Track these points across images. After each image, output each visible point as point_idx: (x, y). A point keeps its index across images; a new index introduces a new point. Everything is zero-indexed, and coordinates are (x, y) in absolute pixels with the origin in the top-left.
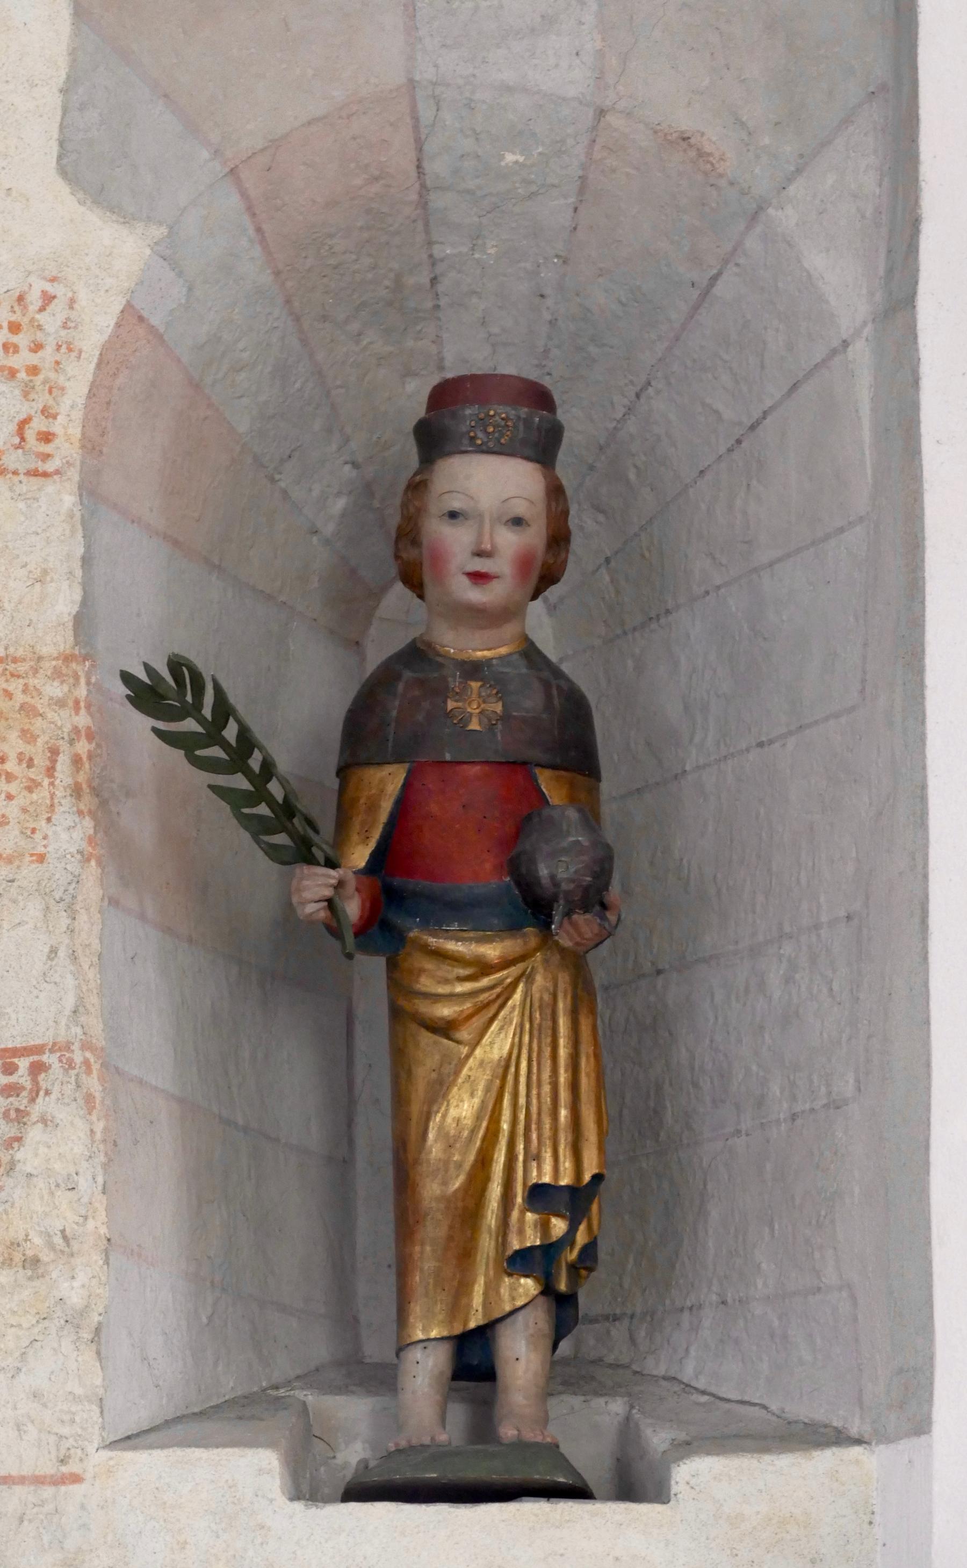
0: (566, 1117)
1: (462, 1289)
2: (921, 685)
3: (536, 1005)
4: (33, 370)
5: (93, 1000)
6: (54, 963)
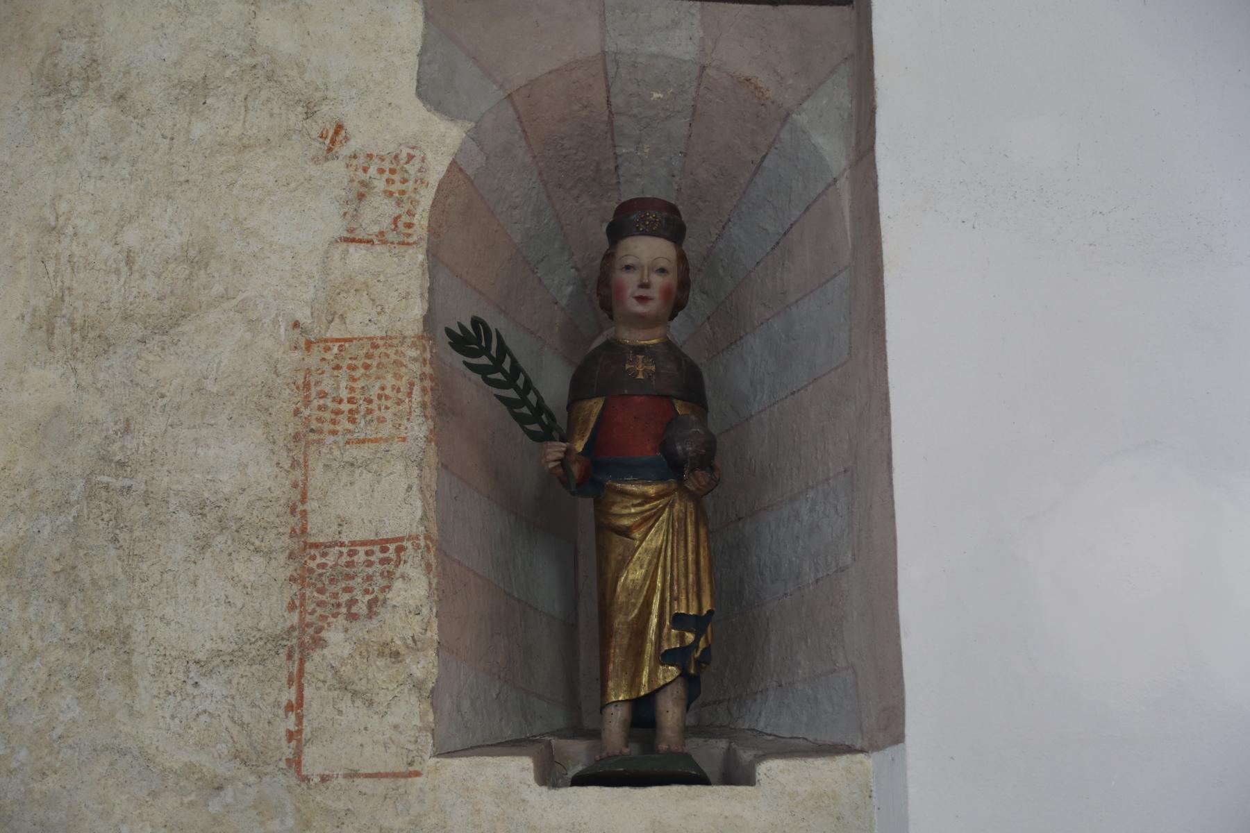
0: (693, 580)
1: (637, 673)
3: (676, 518)
4: (403, 192)
5: (432, 514)
6: (410, 494)
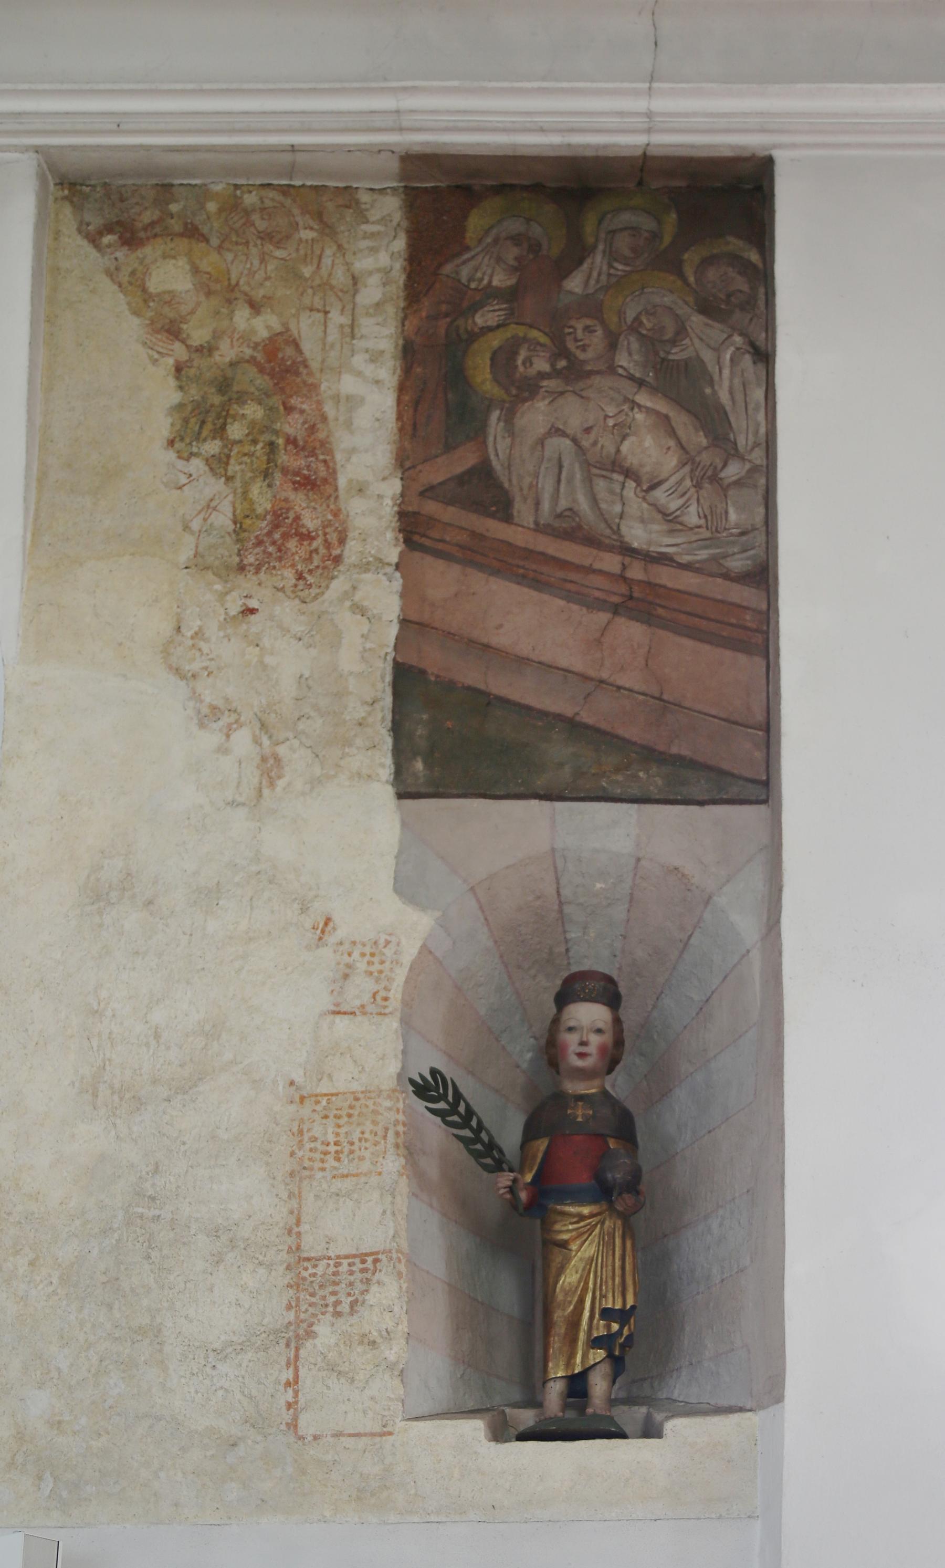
1: (572, 1355)
2: (782, 1081)
4: (381, 972)
